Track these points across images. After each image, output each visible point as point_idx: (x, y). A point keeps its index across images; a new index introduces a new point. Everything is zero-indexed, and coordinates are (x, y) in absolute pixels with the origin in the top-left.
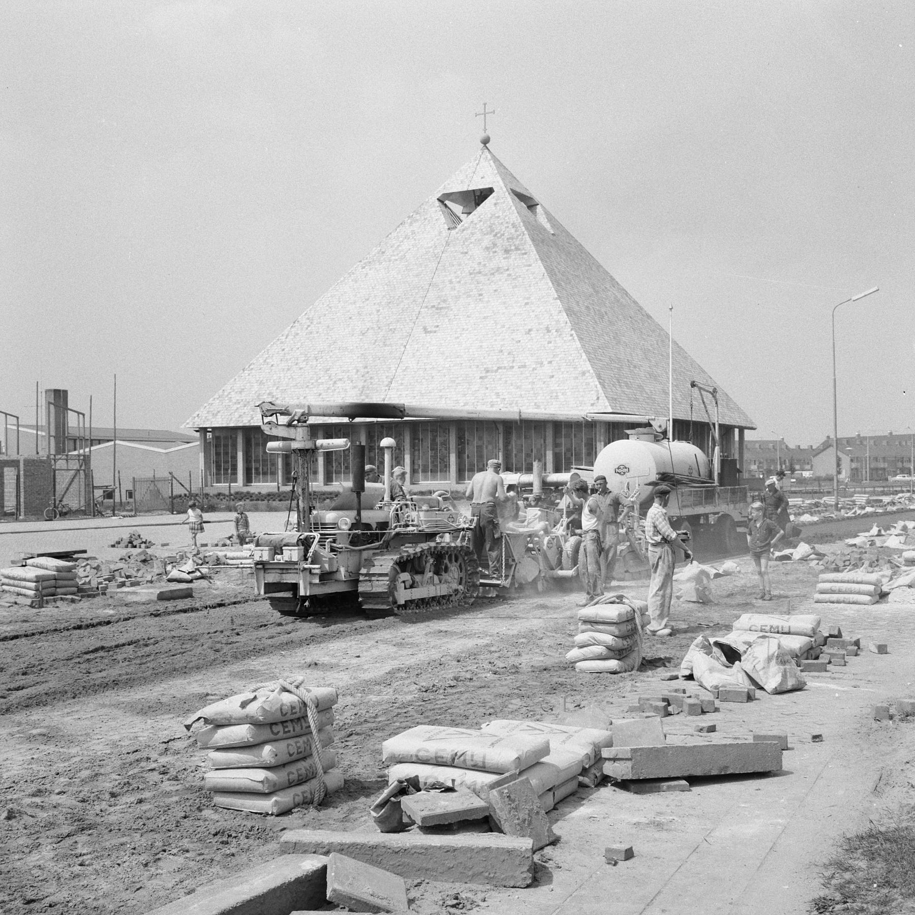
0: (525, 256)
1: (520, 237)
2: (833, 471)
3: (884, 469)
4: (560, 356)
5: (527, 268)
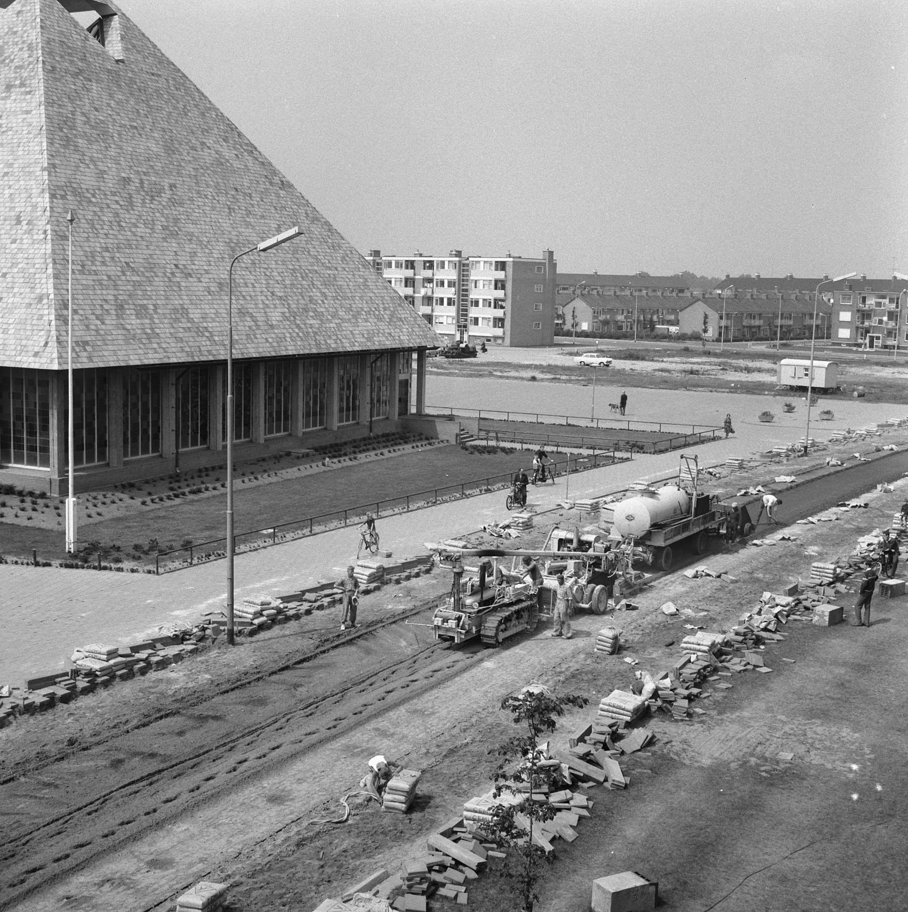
0: (28, 97)
1: (31, 66)
2: (699, 328)
3: (759, 327)
4: (20, 266)
5: (25, 116)
